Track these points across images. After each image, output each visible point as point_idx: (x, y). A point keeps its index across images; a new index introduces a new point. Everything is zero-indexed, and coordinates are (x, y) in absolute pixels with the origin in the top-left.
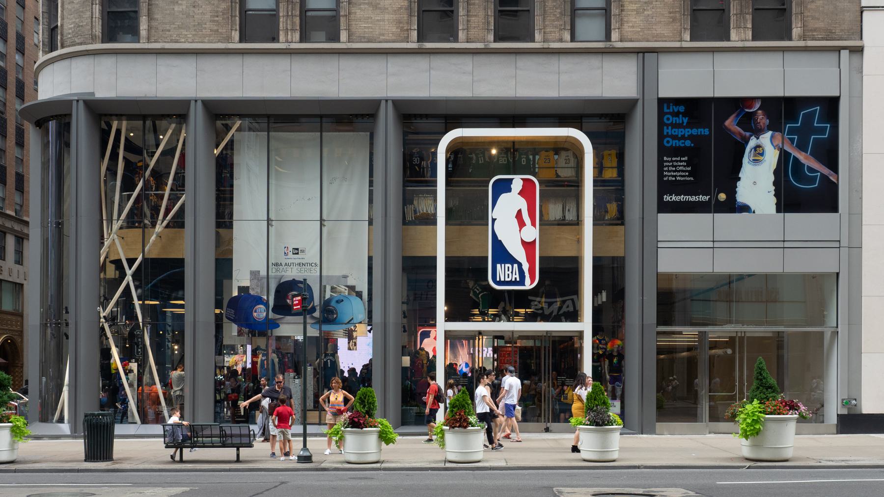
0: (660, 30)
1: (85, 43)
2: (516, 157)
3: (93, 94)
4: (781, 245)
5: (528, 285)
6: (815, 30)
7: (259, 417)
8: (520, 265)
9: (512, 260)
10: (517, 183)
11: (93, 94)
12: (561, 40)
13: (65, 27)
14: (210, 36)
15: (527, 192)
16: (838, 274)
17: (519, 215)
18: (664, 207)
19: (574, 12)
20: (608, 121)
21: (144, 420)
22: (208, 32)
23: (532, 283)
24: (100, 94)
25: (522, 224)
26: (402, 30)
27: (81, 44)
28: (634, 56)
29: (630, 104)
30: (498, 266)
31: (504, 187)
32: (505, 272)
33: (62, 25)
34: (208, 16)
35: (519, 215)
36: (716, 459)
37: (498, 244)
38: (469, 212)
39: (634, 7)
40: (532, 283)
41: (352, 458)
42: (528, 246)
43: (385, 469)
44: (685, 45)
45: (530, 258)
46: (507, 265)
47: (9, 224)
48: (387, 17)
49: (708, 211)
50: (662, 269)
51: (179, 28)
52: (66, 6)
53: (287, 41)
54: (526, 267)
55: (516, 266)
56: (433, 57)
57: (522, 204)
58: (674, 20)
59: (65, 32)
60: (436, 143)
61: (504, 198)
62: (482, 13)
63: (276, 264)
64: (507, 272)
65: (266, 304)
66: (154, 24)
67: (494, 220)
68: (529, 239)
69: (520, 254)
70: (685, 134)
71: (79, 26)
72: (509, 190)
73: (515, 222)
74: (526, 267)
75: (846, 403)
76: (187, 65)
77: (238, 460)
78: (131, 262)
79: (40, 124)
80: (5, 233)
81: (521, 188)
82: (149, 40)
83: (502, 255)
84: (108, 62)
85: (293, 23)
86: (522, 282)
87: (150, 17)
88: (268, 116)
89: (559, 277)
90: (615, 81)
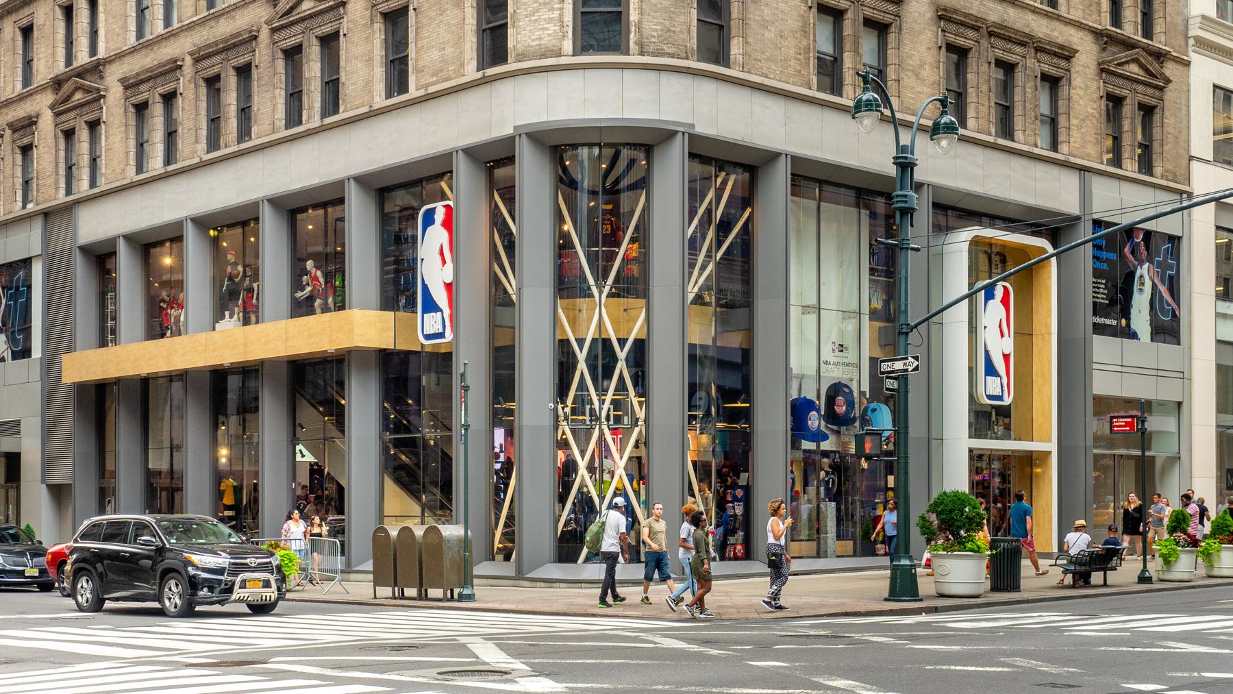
3: (693, 126)
4: (1119, 369)
11: (693, 126)
13: (646, 26)
16: (1180, 404)
18: (1099, 329)
22: (791, 71)
24: (701, 129)
28: (1077, 173)
29: (1078, 218)
34: (792, 52)
36: (838, 605)
41: (1186, 577)
43: (1193, 587)
44: (1037, 151)
49: (1115, 335)
51: (768, 60)
56: (1122, 183)
65: (818, 411)
71: (669, 31)
76: (777, 107)
77: (1105, 585)
78: (622, 342)
84: (709, 87)
88: (821, 182)
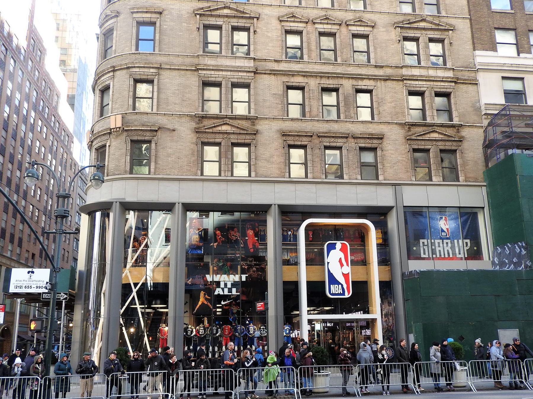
0: (402, 176)
1: (121, 174)
2: (337, 233)
3: (124, 199)
5: (347, 296)
6: (470, 178)
7: (19, 373)
8: (342, 285)
9: (338, 283)
10: (339, 244)
12: (357, 179)
13: (110, 166)
14: (186, 172)
15: (343, 249)
17: (340, 261)
20: (378, 214)
23: (349, 294)
25: (342, 265)
26: (281, 172)
27: (119, 175)
30: (332, 286)
31: (332, 247)
32: (335, 289)
33: (108, 165)
34: (185, 163)
35: (340, 261)
37: (331, 275)
38: (316, 259)
39: (389, 165)
40: (349, 294)
42: (346, 276)
47: (4, 261)
48: (274, 166)
50: (13, 270)
52: (110, 156)
53: (225, 176)
54: (345, 286)
55: (340, 286)
57: (342, 255)
58: (407, 171)
59: (109, 168)
60: (299, 225)
61: (332, 252)
62: (319, 166)
66: (158, 166)
67: (328, 263)
72: (335, 248)
74: (345, 286)
75: (81, 359)
78: (136, 285)
79: (91, 214)
80: (1, 266)
81: (340, 247)
82: (155, 174)
83: (333, 280)
85: (228, 168)
86: (343, 294)
87: (156, 162)
89: (361, 289)
90: (381, 197)
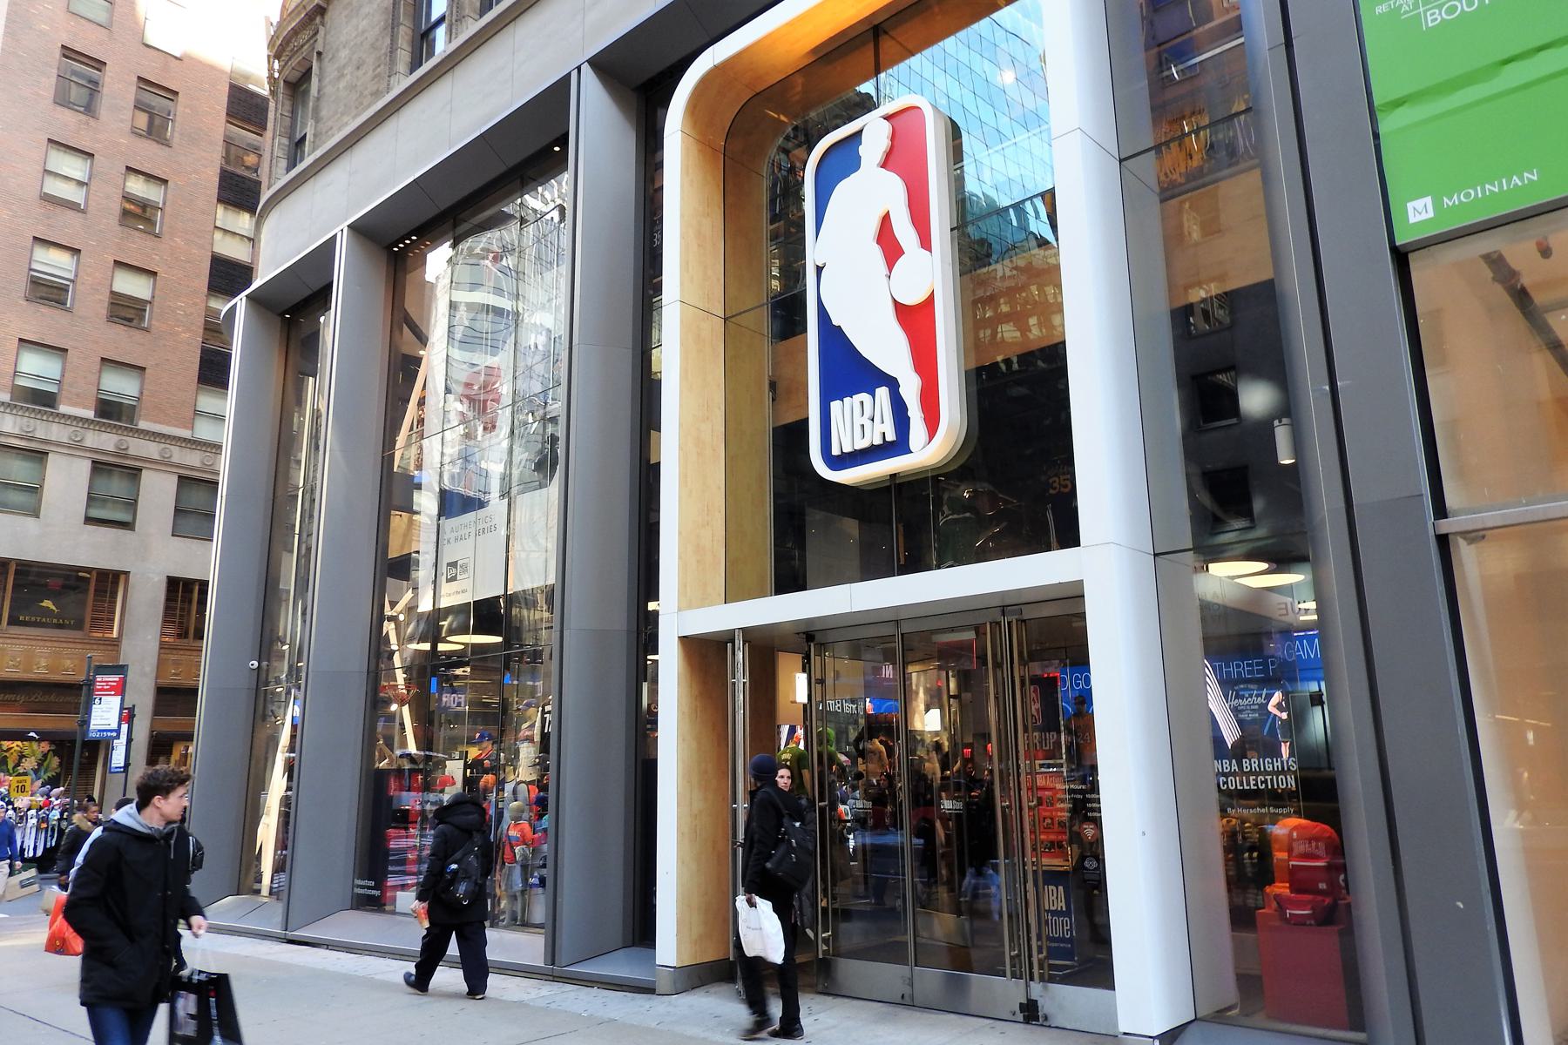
8: (892, 384)
19: (927, 835)
21: (1014, 976)
32: (857, 421)
42: (915, 320)
45: (924, 361)
46: (858, 397)
54: (910, 389)
55: (883, 393)
61: (844, 192)
63: (453, 565)
64: (858, 421)
66: (320, 125)
67: (819, 270)
68: (912, 298)
69: (885, 347)
70: (1239, 132)
73: (877, 253)
74: (910, 389)
83: (850, 371)
86: (899, 446)
